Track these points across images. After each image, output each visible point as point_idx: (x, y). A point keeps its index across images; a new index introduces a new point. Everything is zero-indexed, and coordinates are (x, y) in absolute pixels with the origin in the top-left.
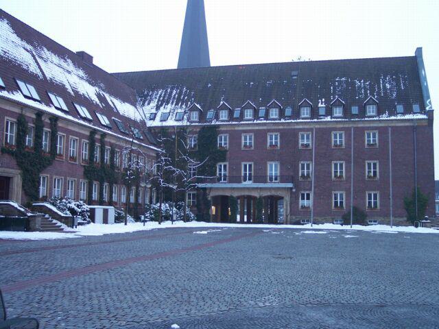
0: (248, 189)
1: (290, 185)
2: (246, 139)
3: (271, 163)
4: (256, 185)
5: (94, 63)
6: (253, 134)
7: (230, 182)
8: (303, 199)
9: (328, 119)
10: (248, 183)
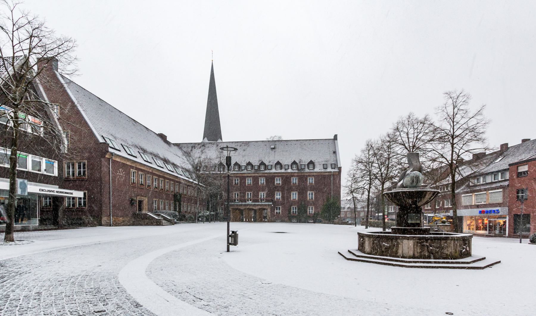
1: (271, 203)
4: (253, 203)
6: (251, 178)
10: (250, 202)
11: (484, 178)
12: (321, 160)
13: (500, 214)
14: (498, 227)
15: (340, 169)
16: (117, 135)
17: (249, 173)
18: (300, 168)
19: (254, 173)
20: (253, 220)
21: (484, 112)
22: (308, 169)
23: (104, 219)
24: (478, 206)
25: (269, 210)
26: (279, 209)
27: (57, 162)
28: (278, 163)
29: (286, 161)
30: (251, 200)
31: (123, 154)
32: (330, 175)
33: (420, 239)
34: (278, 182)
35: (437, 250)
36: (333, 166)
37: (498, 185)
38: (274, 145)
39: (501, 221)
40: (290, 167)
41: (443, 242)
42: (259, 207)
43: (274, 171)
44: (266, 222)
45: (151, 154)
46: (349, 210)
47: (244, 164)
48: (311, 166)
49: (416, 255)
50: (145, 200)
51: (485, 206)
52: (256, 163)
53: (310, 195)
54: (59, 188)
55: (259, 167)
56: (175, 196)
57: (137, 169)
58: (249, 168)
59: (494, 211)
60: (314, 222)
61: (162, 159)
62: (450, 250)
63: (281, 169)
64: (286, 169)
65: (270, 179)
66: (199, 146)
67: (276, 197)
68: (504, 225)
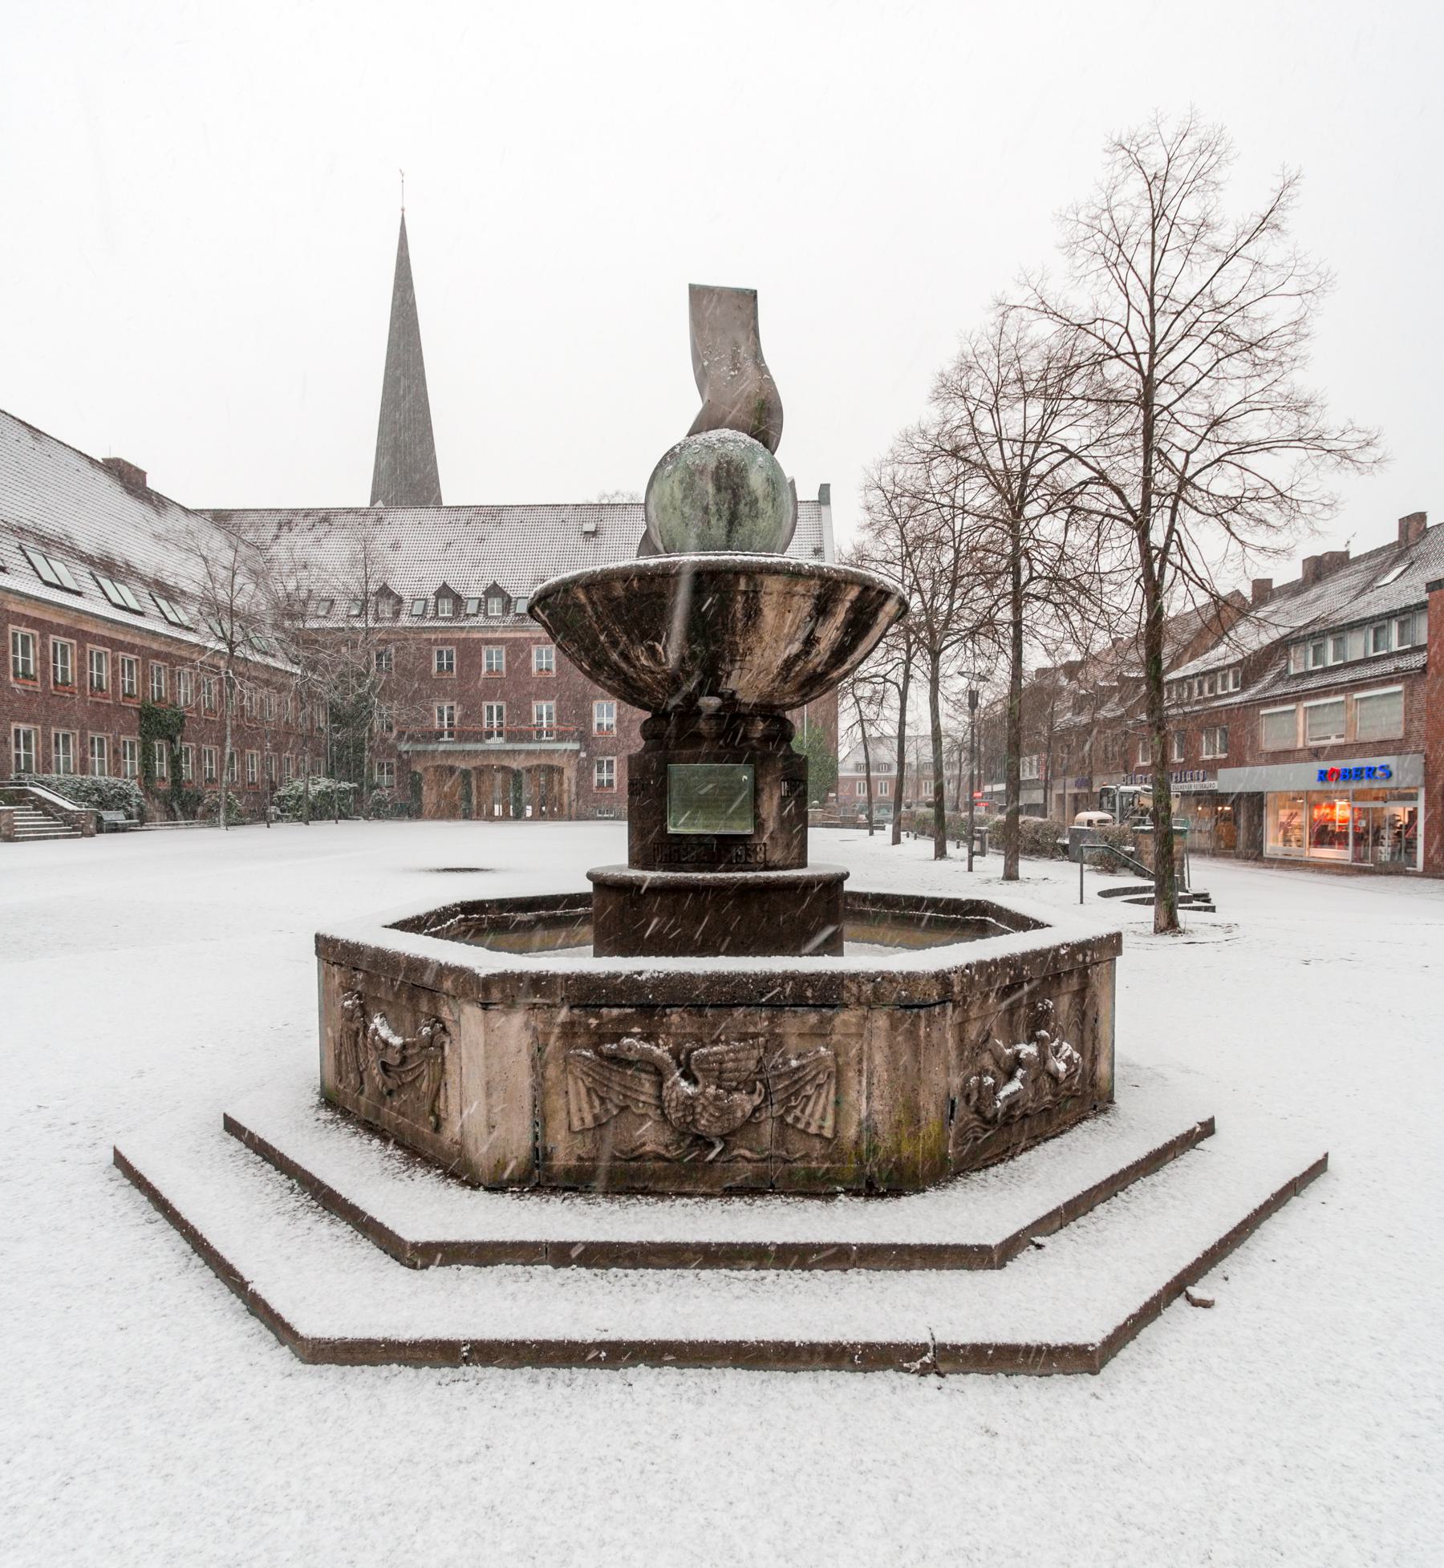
1: (576, 746)
2: (540, 656)
4: (459, 747)
5: (149, 485)
6: (503, 649)
7: (509, 740)
8: (600, 770)
10: (496, 743)
11: (1339, 641)
13: (1393, 783)
14: (1387, 833)
20: (498, 810)
21: (1290, 218)
24: (1316, 754)
25: (570, 773)
30: (500, 734)
33: (587, 993)
35: (744, 1102)
37: (1389, 666)
39: (1400, 811)
41: (793, 1024)
49: (564, 1153)
51: (1339, 751)
58: (495, 605)
59: (1371, 771)
61: (87, 560)
62: (862, 1103)
66: (310, 520)
67: (596, 720)
68: (1408, 827)
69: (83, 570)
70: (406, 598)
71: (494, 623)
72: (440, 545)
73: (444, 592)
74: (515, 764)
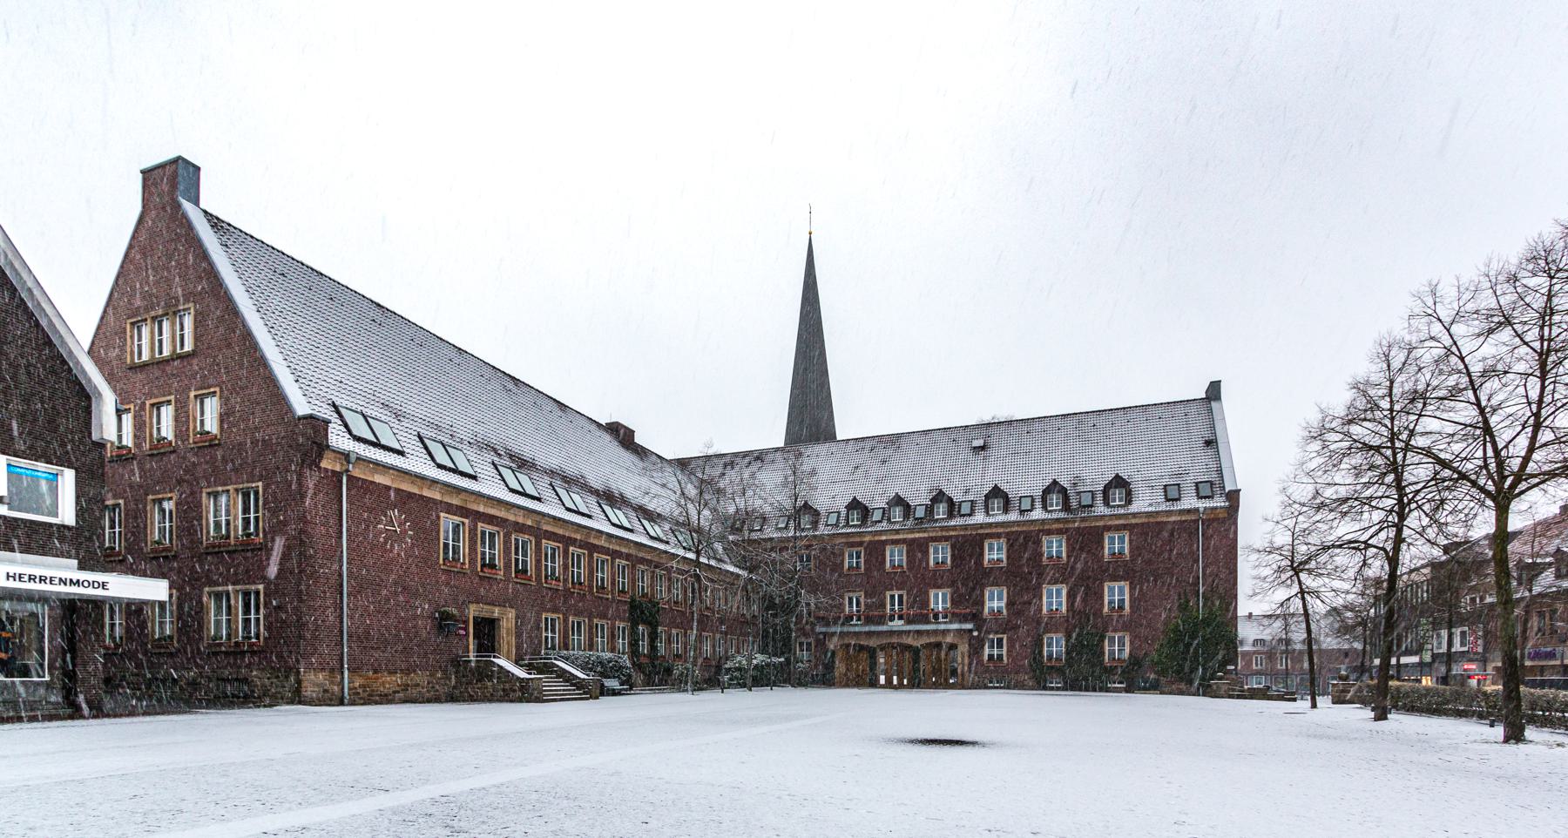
0: (900, 633)
1: (969, 626)
2: (936, 552)
3: (1112, 584)
9: (884, 525)
10: (897, 624)
12: (1155, 477)
15: (1233, 497)
16: (410, 408)
17: (897, 532)
18: (1074, 503)
19: (911, 531)
20: (882, 679)
22: (1106, 503)
23: (313, 681)
25: (963, 648)
26: (1000, 646)
27: (72, 472)
28: (996, 492)
29: (1025, 482)
30: (900, 618)
31: (417, 463)
32: (1189, 525)
34: (995, 553)
36: (1205, 491)
38: (982, 439)
40: (1038, 505)
42: (925, 640)
43: (980, 518)
44: (952, 687)
45: (552, 473)
46: (1259, 648)
47: (880, 503)
48: (1117, 496)
50: (508, 620)
52: (918, 497)
53: (1116, 593)
54: (81, 567)
55: (930, 510)
56: (633, 606)
57: (462, 511)
58: (897, 514)
60: (1127, 690)
61: (596, 492)
63: (1006, 510)
64: (1022, 512)
65: (968, 545)
66: (747, 460)
67: (987, 605)
69: (592, 500)
70: (823, 512)
71: (897, 527)
72: (849, 469)
73: (854, 505)
74: (873, 643)
